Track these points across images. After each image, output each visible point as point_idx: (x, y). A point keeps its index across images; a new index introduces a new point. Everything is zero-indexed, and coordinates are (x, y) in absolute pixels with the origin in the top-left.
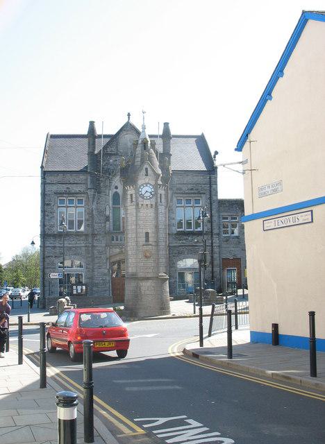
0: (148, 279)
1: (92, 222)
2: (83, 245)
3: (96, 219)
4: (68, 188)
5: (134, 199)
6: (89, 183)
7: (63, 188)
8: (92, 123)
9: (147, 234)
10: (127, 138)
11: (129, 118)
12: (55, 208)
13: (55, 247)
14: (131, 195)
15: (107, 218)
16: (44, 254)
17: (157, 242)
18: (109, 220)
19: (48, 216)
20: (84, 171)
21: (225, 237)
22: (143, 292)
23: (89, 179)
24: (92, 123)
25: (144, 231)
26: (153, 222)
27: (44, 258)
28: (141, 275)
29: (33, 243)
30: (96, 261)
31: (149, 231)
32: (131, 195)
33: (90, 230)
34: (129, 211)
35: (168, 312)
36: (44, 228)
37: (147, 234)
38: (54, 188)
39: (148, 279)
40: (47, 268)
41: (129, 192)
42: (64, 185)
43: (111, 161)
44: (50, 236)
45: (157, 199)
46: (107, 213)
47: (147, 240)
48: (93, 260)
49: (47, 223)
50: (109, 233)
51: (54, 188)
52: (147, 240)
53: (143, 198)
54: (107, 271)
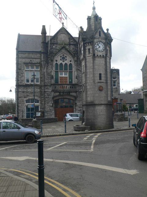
0: (101, 105)
1: (44, 79)
2: (39, 91)
3: (46, 77)
4: (31, 61)
5: (91, 52)
6: (42, 58)
7: (28, 61)
8: (44, 27)
9: (100, 74)
10: (62, 37)
11: (63, 25)
12: (24, 71)
13: (24, 92)
14: (89, 49)
15: (52, 77)
16: (18, 96)
17: (107, 80)
18: (53, 78)
19: (20, 75)
20: (40, 52)
21: (114, 88)
22: (98, 113)
23: (42, 56)
24: (44, 27)
25: (99, 73)
26: (104, 67)
27: (18, 98)
28: (97, 102)
29: (11, 91)
30: (46, 99)
31: (101, 73)
32: (89, 49)
33: (43, 84)
34: (87, 60)
35: (113, 127)
36: (18, 81)
37: (100, 74)
38: (24, 60)
39: (101, 105)
40: (20, 103)
41: (87, 48)
42: (29, 59)
43: (54, 47)
44: (21, 86)
45: (106, 52)
46: (52, 74)
47: (100, 79)
48: (45, 98)
49: (19, 79)
50: (54, 85)
51: (24, 60)
52: (100, 79)
53: (98, 51)
54: (52, 105)
